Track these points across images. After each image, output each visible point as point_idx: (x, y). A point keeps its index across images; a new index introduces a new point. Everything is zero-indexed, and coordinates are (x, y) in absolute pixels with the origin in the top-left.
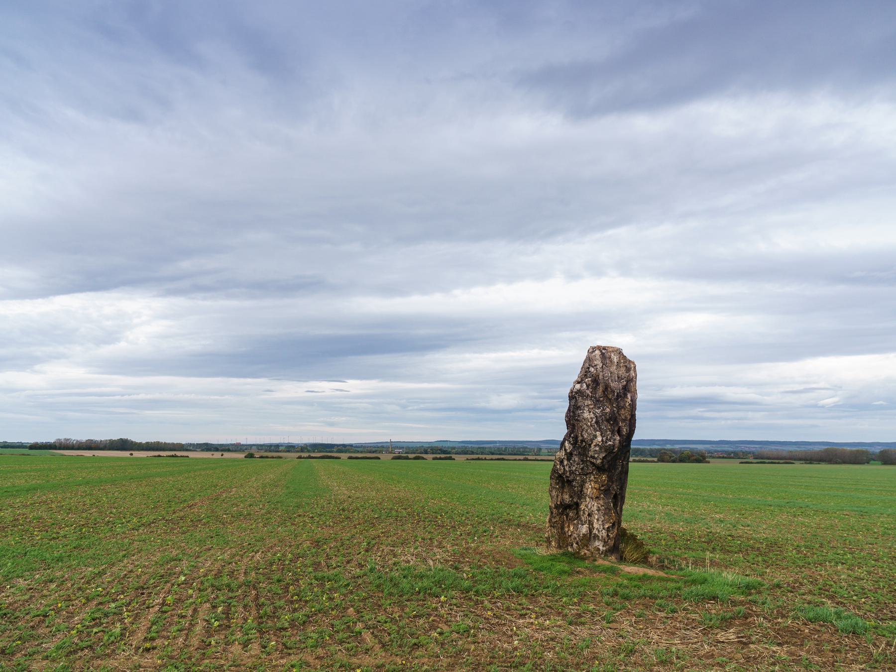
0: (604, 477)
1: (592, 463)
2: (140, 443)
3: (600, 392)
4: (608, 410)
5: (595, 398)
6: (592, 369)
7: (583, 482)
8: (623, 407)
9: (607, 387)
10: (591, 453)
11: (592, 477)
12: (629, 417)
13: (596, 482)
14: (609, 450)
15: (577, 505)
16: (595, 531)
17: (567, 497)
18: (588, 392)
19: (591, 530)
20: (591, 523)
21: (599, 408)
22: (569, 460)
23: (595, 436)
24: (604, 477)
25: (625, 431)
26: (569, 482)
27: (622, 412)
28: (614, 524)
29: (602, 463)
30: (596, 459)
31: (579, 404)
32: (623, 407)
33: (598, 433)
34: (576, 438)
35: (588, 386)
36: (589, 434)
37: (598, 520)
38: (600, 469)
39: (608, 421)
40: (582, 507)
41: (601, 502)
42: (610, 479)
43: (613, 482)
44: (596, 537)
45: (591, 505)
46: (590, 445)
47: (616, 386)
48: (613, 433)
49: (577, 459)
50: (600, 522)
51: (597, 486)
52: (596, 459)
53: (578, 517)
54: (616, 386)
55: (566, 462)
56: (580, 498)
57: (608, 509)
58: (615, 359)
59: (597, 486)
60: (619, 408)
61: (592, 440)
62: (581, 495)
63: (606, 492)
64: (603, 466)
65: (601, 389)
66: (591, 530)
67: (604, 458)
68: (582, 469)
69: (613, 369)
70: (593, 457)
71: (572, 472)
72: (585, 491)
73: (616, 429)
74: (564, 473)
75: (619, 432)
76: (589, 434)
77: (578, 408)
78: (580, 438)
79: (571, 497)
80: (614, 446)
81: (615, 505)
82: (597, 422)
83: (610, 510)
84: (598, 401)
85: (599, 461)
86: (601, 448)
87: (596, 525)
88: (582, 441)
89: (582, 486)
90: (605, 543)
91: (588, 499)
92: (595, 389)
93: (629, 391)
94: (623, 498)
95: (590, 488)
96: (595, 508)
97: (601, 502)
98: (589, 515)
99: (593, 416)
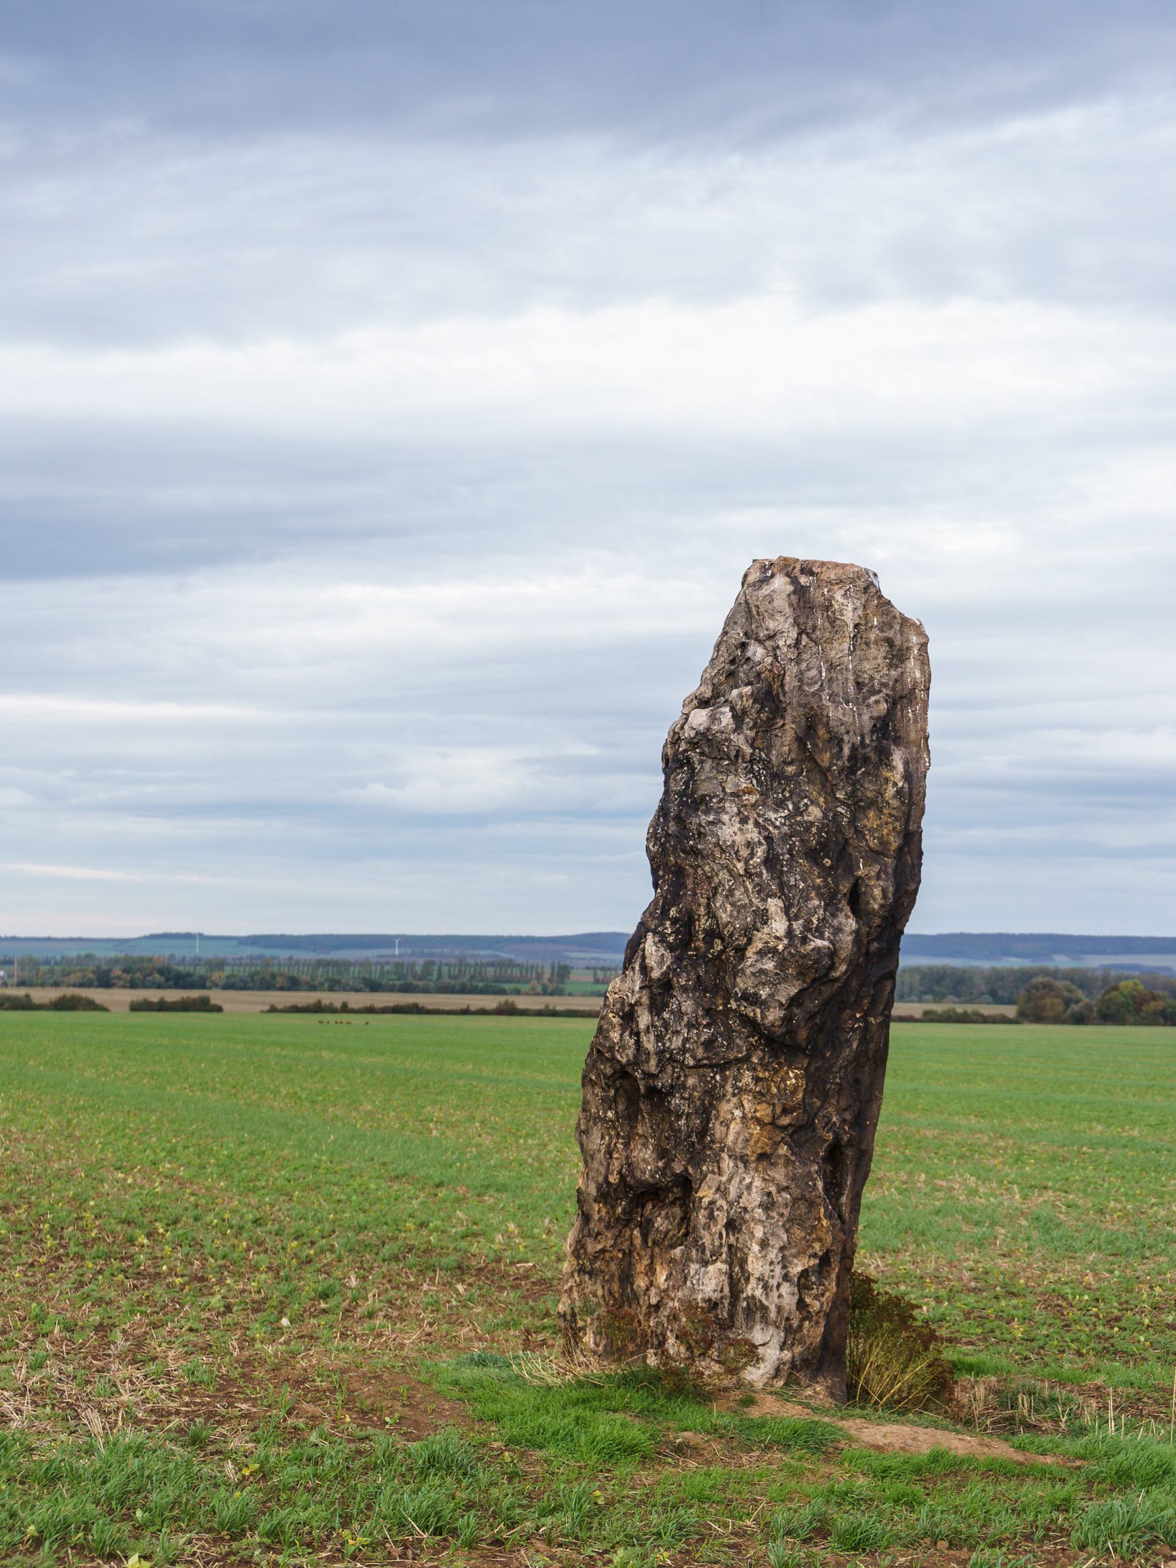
0: (793, 1077)
1: (747, 1021)
5: (767, 764)
6: (757, 652)
7: (711, 1099)
8: (872, 803)
9: (812, 723)
10: (743, 984)
11: (747, 1078)
12: (895, 842)
13: (760, 1097)
14: (815, 972)
16: (753, 1289)
17: (645, 1158)
19: (735, 1284)
20: (736, 1258)
21: (780, 804)
22: (656, 1008)
23: (763, 917)
24: (793, 1077)
25: (877, 895)
26: (658, 1097)
27: (871, 820)
29: (786, 1020)
31: (704, 789)
33: (774, 905)
34: (687, 922)
36: (739, 908)
37: (764, 1244)
38: (778, 1045)
39: (813, 855)
40: (706, 1193)
42: (816, 1084)
44: (756, 1311)
45: (741, 1186)
46: (741, 951)
47: (850, 718)
48: (831, 903)
49: (688, 1006)
50: (773, 1254)
51: (764, 1111)
54: (850, 718)
55: (644, 1019)
56: (696, 1158)
57: (804, 1200)
61: (748, 933)
62: (700, 1145)
63: (799, 1134)
64: (791, 1032)
66: (735, 1284)
67: (794, 1001)
68: (709, 1044)
70: (751, 999)
71: (667, 1058)
72: (719, 1131)
73: (845, 887)
75: (856, 900)
76: (739, 908)
78: (704, 923)
79: (662, 1153)
80: (833, 954)
82: (771, 861)
83: (812, 1205)
84: (778, 776)
85: (774, 1015)
86: (782, 964)
87: (756, 1266)
88: (712, 934)
89: (706, 1111)
90: (791, 1334)
91: (727, 1163)
92: (765, 730)
95: (737, 1120)
96: (753, 1199)
97: (779, 1174)
98: (732, 1225)
99: (754, 835)
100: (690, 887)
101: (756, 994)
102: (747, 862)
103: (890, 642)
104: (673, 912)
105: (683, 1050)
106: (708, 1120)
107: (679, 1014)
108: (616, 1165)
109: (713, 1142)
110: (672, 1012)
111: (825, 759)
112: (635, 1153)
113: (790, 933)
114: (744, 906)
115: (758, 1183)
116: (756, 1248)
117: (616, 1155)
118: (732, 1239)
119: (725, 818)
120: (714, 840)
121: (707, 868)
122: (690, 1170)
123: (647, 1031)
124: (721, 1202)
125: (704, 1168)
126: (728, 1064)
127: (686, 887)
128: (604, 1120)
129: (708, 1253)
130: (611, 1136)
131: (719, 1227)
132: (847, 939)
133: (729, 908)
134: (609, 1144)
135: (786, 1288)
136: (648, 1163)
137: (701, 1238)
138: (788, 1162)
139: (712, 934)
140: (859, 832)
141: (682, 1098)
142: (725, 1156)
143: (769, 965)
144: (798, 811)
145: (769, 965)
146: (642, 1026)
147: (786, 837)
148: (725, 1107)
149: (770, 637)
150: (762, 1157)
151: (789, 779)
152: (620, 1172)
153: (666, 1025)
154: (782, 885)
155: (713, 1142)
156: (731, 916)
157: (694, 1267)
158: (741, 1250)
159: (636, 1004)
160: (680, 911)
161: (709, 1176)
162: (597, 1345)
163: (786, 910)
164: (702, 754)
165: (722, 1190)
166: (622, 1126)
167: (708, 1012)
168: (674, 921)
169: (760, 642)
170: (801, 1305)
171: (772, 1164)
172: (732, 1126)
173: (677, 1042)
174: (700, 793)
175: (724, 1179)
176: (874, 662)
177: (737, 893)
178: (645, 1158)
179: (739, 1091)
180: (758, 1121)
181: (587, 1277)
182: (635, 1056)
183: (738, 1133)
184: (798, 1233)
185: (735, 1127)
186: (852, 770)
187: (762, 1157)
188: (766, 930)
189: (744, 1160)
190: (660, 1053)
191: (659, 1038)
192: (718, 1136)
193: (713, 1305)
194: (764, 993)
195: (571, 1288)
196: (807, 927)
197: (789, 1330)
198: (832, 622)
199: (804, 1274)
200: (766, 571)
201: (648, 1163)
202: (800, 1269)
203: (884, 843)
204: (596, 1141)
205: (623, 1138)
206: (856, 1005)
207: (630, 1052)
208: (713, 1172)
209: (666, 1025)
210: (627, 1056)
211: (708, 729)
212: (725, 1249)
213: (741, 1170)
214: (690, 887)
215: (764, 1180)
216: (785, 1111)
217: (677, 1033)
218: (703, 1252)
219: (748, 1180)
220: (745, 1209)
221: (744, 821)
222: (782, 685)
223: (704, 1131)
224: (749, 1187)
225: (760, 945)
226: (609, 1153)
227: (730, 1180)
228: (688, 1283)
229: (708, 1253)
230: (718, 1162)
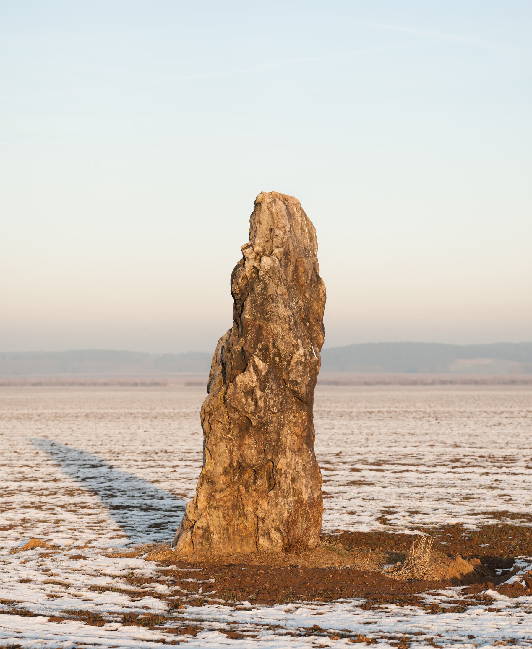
7: (281, 425)
10: (293, 376)
17: (251, 454)
37: (306, 486)
51: (297, 431)
55: (258, 393)
56: (276, 453)
62: (277, 448)
71: (268, 409)
72: (284, 440)
76: (288, 344)
91: (289, 454)
96: (300, 467)
98: (293, 480)
100: (265, 334)
101: (296, 380)
102: (289, 324)
104: (259, 346)
105: (273, 406)
106: (279, 435)
107: (272, 390)
108: (235, 459)
109: (282, 445)
110: (269, 389)
112: (245, 452)
114: (289, 343)
115: (300, 461)
116: (304, 488)
117: (234, 454)
118: (294, 486)
119: (280, 305)
120: (277, 314)
121: (272, 326)
122: (274, 458)
123: (260, 398)
124: (289, 470)
125: (280, 456)
127: (263, 335)
128: (226, 439)
129: (286, 492)
130: (230, 446)
133: (283, 344)
134: (230, 449)
136: (253, 456)
137: (283, 486)
141: (272, 427)
142: (287, 450)
146: (258, 396)
148: (285, 429)
149: (283, 227)
152: (238, 461)
153: (267, 395)
155: (282, 445)
156: (285, 347)
157: (280, 499)
158: (298, 490)
159: (255, 387)
160: (262, 345)
161: (282, 459)
162: (220, 539)
164: (270, 277)
166: (236, 441)
168: (260, 350)
169: (280, 229)
171: (302, 452)
172: (288, 437)
173: (271, 403)
174: (269, 293)
175: (289, 460)
177: (286, 337)
178: (251, 454)
180: (296, 434)
181: (213, 509)
182: (255, 410)
183: (290, 440)
185: (289, 437)
188: (298, 353)
190: (265, 408)
191: (265, 401)
192: (284, 442)
194: (299, 380)
195: (206, 515)
201: (253, 456)
202: (317, 495)
205: (237, 446)
207: (253, 408)
208: (283, 458)
209: (267, 395)
210: (251, 409)
211: (274, 266)
212: (291, 490)
213: (294, 456)
214: (265, 334)
215: (302, 459)
217: (271, 398)
218: (284, 492)
219: (297, 460)
220: (298, 472)
221: (286, 306)
222: (289, 248)
223: (278, 440)
224: (297, 463)
225: (296, 360)
226: (231, 452)
227: (291, 460)
228: (279, 506)
229: (286, 492)
230: (285, 453)
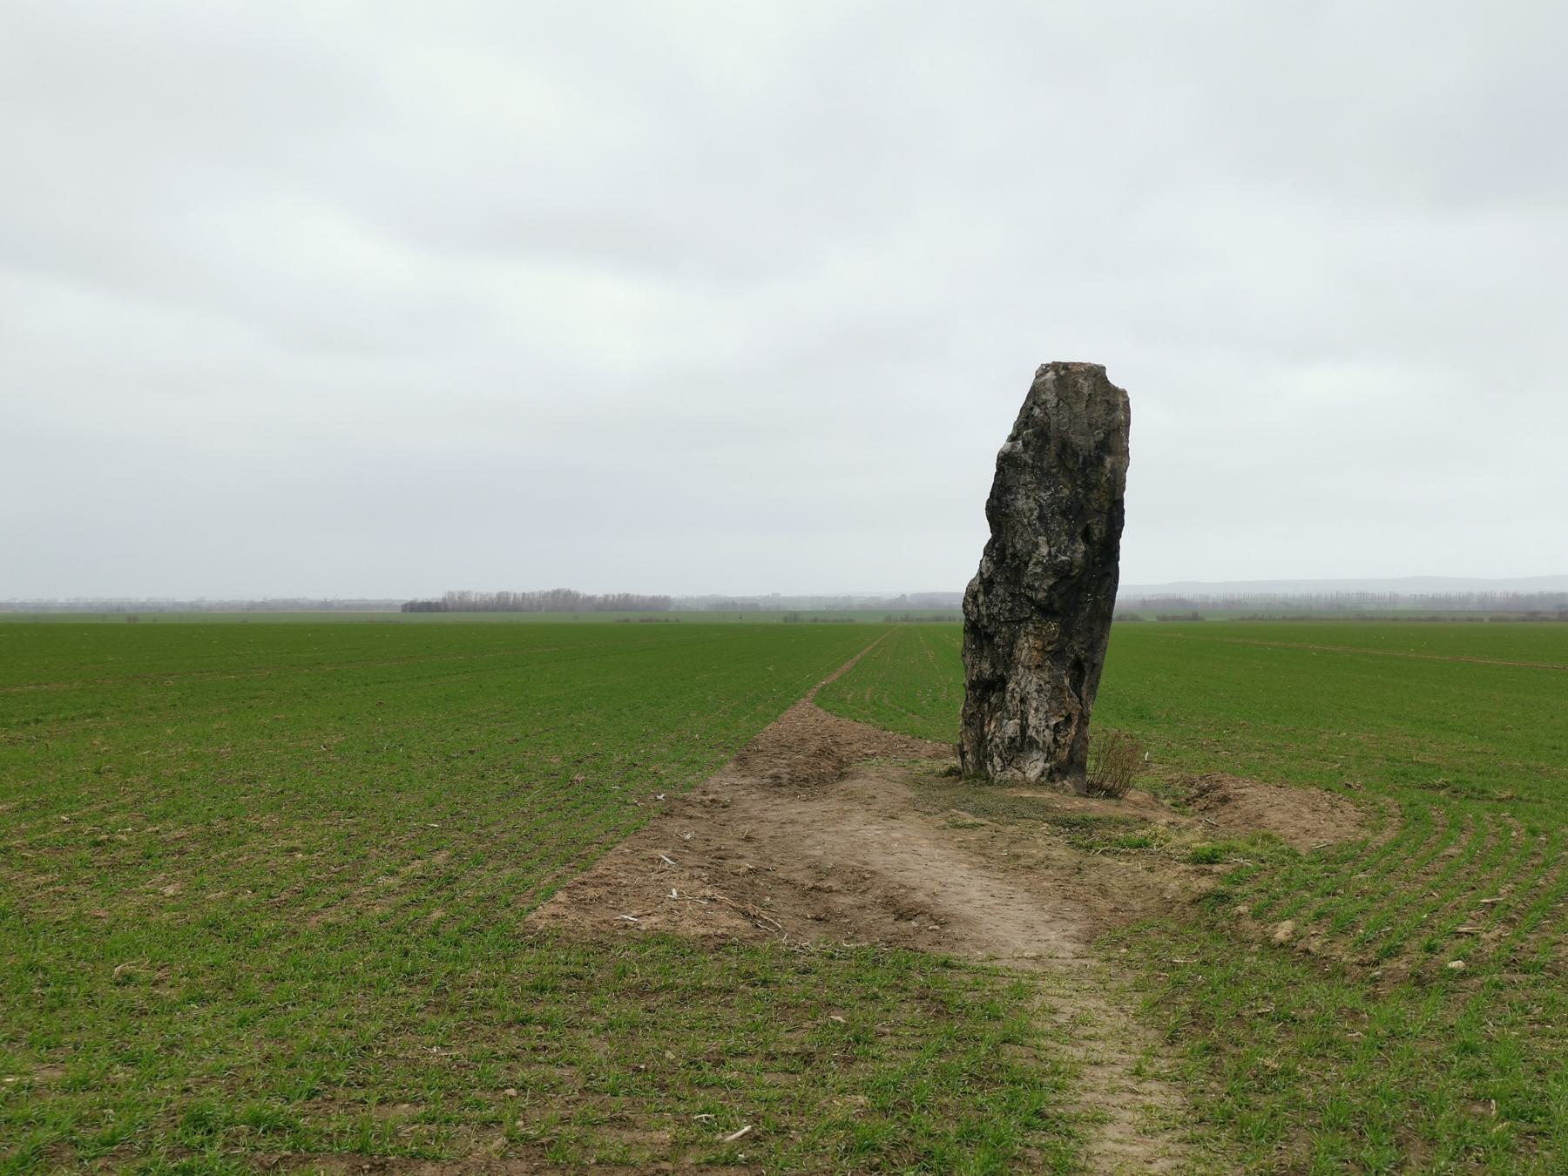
1: (1030, 599)
2: (591, 599)
3: (1051, 458)
4: (1066, 492)
5: (1041, 469)
7: (1014, 637)
9: (1065, 445)
10: (1026, 580)
12: (1107, 506)
13: (1037, 637)
14: (1063, 574)
15: (1003, 681)
16: (1031, 732)
18: (1027, 457)
19: (1023, 728)
20: (1024, 717)
21: (1048, 488)
22: (987, 593)
23: (1036, 546)
25: (1097, 532)
26: (990, 637)
27: (1094, 495)
28: (1068, 719)
30: (1036, 590)
32: (1095, 486)
33: (1042, 539)
34: (1003, 550)
35: (1025, 445)
36: (1025, 542)
37: (1037, 710)
38: (1046, 611)
39: (1064, 513)
40: (1011, 686)
41: (1045, 675)
42: (1066, 630)
43: (1071, 637)
44: (1033, 744)
45: (1027, 682)
46: (1026, 564)
48: (1072, 539)
49: (1001, 591)
51: (1039, 644)
52: (1036, 590)
53: (1001, 705)
54: (1084, 442)
55: (981, 598)
56: (1007, 667)
57: (1058, 689)
58: (1086, 387)
59: (1039, 644)
60: (1089, 487)
61: (1030, 554)
62: (1008, 661)
63: (1057, 655)
64: (1051, 604)
65: (1053, 447)
66: (1023, 728)
67: (1051, 588)
68: (1011, 611)
69: (1080, 407)
70: (1031, 587)
72: (1017, 653)
73: (1080, 530)
74: (978, 620)
75: (1086, 536)
77: (1008, 490)
79: (993, 665)
80: (1071, 564)
81: (1077, 684)
82: (1041, 518)
83: (1062, 691)
84: (1047, 474)
85: (1041, 595)
86: (1045, 569)
87: (1032, 721)
88: (1014, 556)
89: (1012, 643)
90: (1050, 755)
91: (1021, 670)
92: (1040, 450)
93: (1110, 453)
94: (1096, 668)
95: (1026, 648)
96: (1033, 687)
97: (1045, 675)
98: (1022, 701)
99: (1032, 504)
103: (1108, 402)
111: (1070, 465)
113: (1049, 553)
126: (1021, 621)
131: (1016, 702)
132: (1079, 556)
135: (1047, 732)
138: (1050, 669)
139: (1014, 556)
140: (1089, 501)
143: (1039, 570)
144: (1057, 491)
145: (1039, 570)
147: (1049, 505)
150: (1038, 666)
151: (1054, 475)
154: (1046, 529)
163: (1048, 542)
165: (1018, 683)
167: (1011, 595)
170: (1055, 740)
176: (1099, 410)
179: (1027, 634)
184: (1054, 704)
186: (1084, 469)
187: (1038, 666)
189: (1029, 668)
193: (1013, 740)
196: (1059, 551)
197: (1049, 753)
198: (1077, 393)
199: (1057, 725)
200: (1044, 370)
203: (1101, 506)
204: (968, 660)
206: (1088, 590)
216: (1050, 643)
223: (1010, 655)
